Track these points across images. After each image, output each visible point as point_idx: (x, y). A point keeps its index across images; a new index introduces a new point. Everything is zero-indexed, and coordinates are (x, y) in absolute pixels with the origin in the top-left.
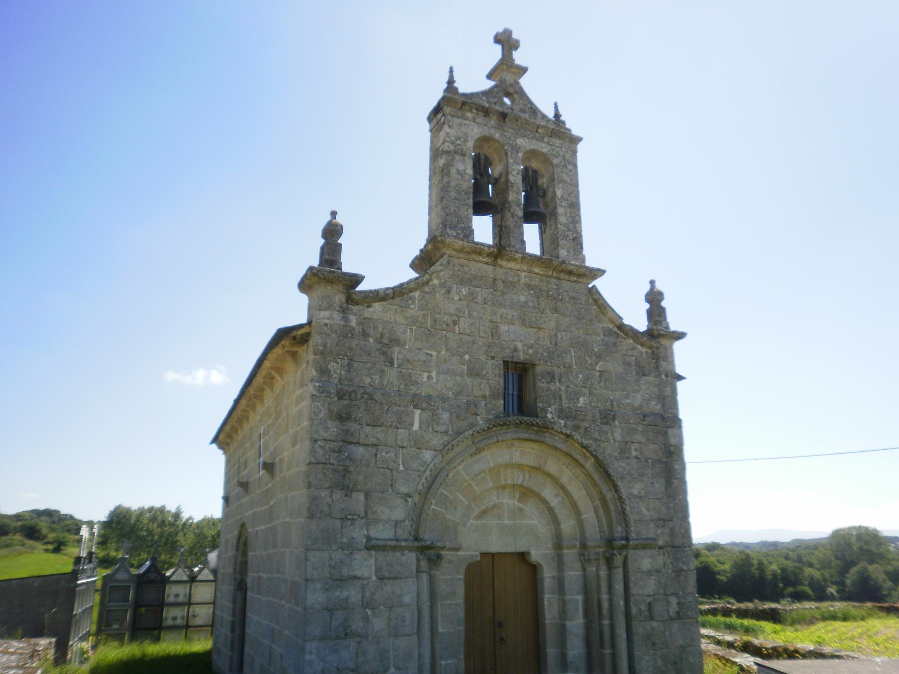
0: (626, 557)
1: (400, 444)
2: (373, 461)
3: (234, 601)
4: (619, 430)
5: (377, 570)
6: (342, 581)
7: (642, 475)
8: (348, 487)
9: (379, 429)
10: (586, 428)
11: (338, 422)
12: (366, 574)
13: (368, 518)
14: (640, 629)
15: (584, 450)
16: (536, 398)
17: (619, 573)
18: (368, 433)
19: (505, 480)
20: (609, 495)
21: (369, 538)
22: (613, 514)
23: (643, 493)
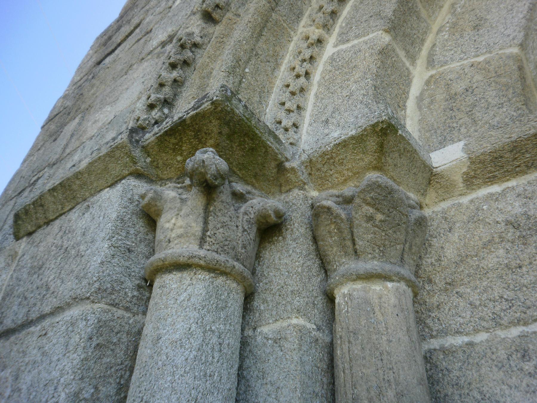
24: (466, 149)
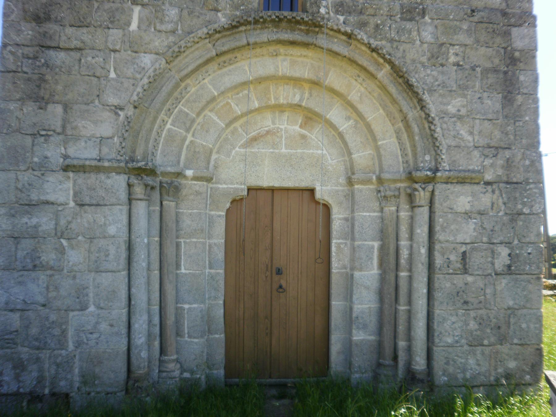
0: (433, 192)
1: (111, 47)
2: (77, 67)
4: (430, 29)
5: (75, 195)
6: (32, 206)
7: (463, 88)
8: (43, 98)
9: (85, 30)
10: (377, 26)
11: (34, 24)
12: (62, 200)
13: (66, 133)
14: (445, 284)
15: (375, 55)
17: (423, 214)
18: (70, 35)
19: (276, 99)
20: (413, 114)
21: (66, 157)
22: (417, 138)
23: (463, 112)
24: (193, 173)
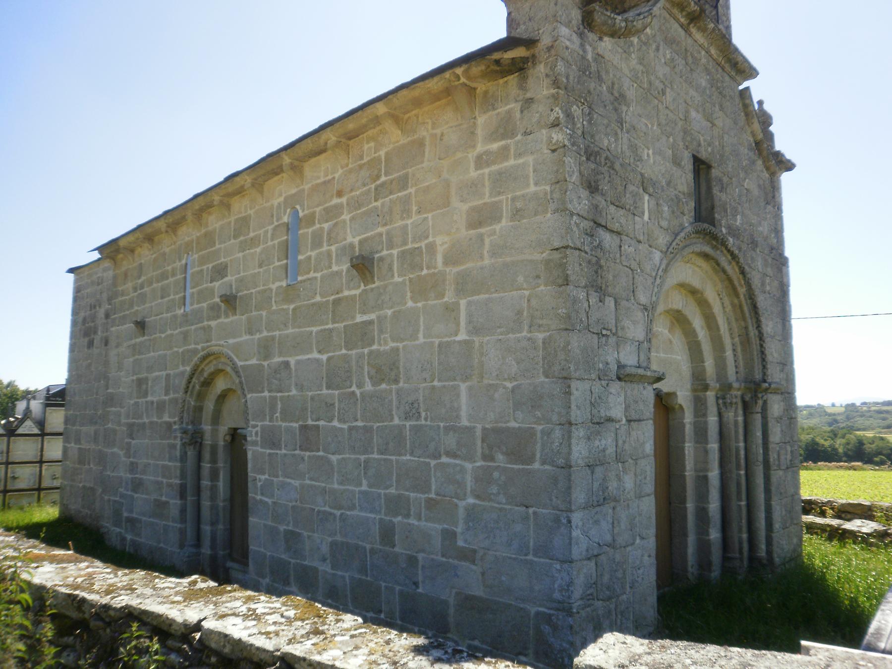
3: (183, 458)
16: (713, 208)
20: (753, 332)
